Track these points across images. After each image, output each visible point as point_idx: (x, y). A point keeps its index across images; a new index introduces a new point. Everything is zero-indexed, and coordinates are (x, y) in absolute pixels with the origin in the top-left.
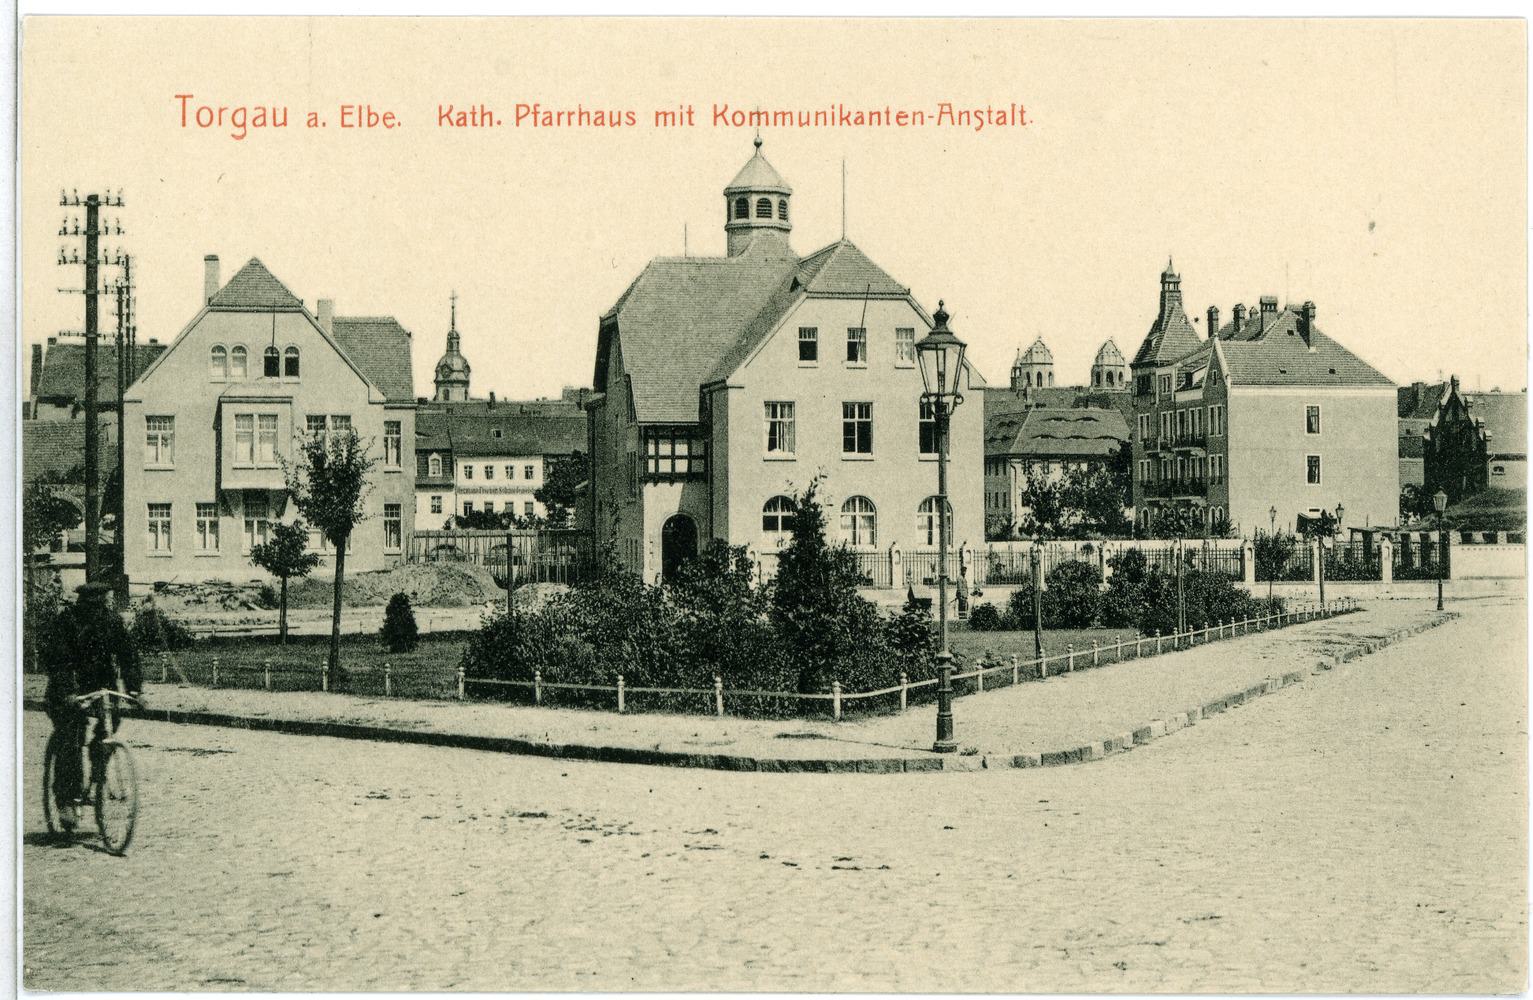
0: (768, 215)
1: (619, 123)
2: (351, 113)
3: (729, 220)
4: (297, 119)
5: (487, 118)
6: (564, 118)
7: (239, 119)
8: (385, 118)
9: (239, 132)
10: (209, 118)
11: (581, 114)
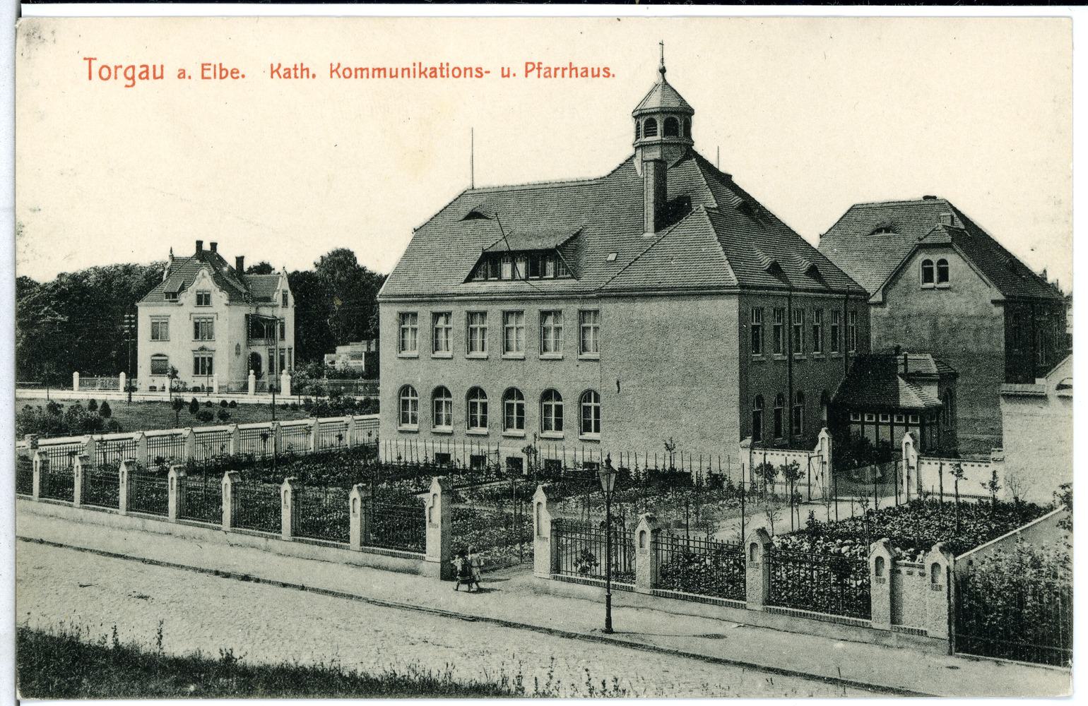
0: (676, 133)
1: (598, 76)
2: (209, 69)
3: (637, 137)
4: (171, 72)
5: (305, 72)
6: (559, 72)
7: (129, 74)
8: (232, 73)
9: (130, 82)
10: (108, 73)
11: (571, 69)
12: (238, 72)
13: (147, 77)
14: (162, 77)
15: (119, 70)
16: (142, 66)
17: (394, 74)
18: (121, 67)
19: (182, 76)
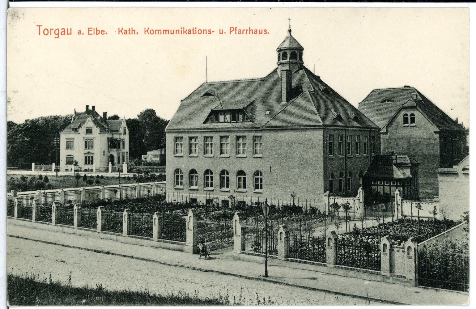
0: (296, 58)
1: (262, 33)
2: (92, 30)
3: (279, 60)
4: (75, 32)
5: (133, 32)
6: (245, 32)
7: (57, 32)
8: (102, 32)
9: (57, 36)
10: (47, 32)
11: (250, 30)
12: (104, 32)
13: (64, 34)
14: (71, 34)
15: (52, 31)
16: (62, 29)
17: (172, 32)
18: (53, 29)
19: (80, 33)
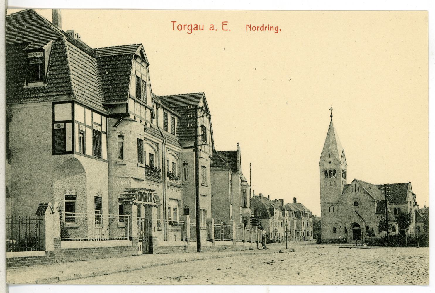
9: (277, 31)
10: (181, 27)
13: (197, 30)
14: (203, 29)
15: (259, 28)
16: (195, 25)
17: (272, 28)
18: (186, 25)
19: (212, 29)
